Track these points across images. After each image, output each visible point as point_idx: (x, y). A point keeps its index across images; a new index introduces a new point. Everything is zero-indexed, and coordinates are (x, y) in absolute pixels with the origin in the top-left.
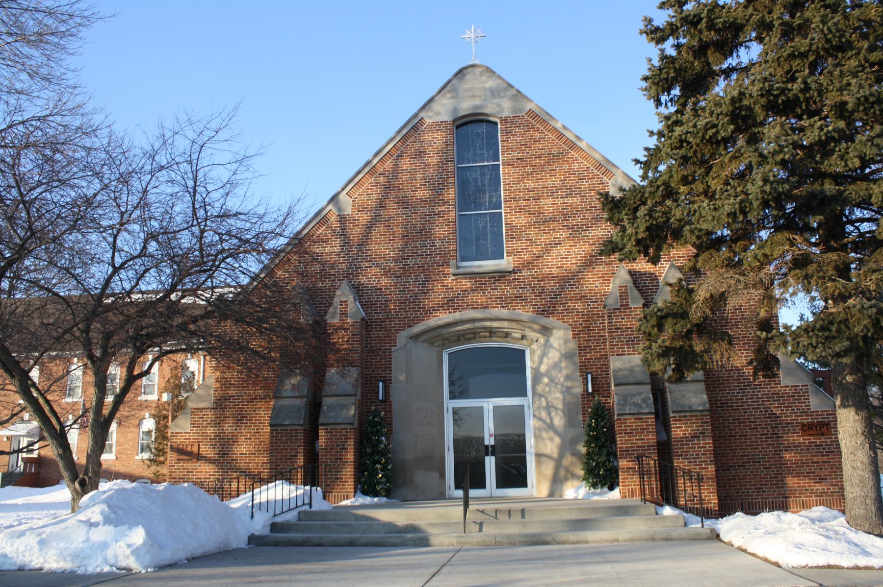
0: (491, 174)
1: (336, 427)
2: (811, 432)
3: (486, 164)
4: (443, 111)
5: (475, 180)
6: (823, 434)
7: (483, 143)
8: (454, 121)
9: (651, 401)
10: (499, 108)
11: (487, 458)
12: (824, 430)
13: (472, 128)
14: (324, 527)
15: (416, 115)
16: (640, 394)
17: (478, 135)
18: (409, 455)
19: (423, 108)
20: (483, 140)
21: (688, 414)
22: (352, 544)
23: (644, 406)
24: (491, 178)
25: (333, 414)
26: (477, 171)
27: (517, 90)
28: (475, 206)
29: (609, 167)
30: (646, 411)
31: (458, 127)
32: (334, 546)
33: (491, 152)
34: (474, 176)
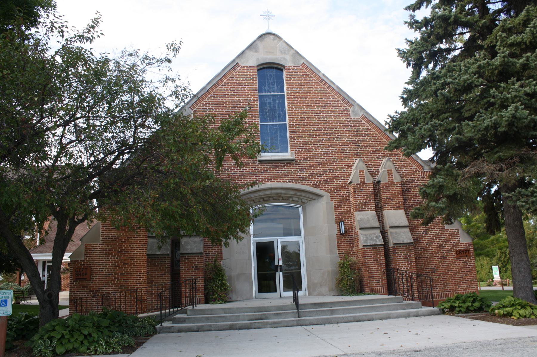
0: (279, 101)
1: (191, 255)
2: (461, 255)
3: (276, 94)
4: (253, 60)
5: (270, 103)
6: (467, 256)
7: (274, 81)
8: (257, 66)
9: (381, 238)
10: (288, 62)
11: (277, 274)
12: (467, 254)
13: (271, 71)
14: (208, 319)
15: (234, 61)
16: (374, 234)
17: (270, 76)
18: (233, 274)
19: (238, 57)
20: (274, 79)
21: (401, 245)
22: (231, 328)
23: (377, 240)
24: (279, 102)
25: (189, 247)
26: (270, 98)
27: (296, 51)
28: (270, 119)
29: (350, 101)
30: (379, 243)
31: (258, 70)
32: (223, 330)
33: (279, 87)
34: (269, 101)
